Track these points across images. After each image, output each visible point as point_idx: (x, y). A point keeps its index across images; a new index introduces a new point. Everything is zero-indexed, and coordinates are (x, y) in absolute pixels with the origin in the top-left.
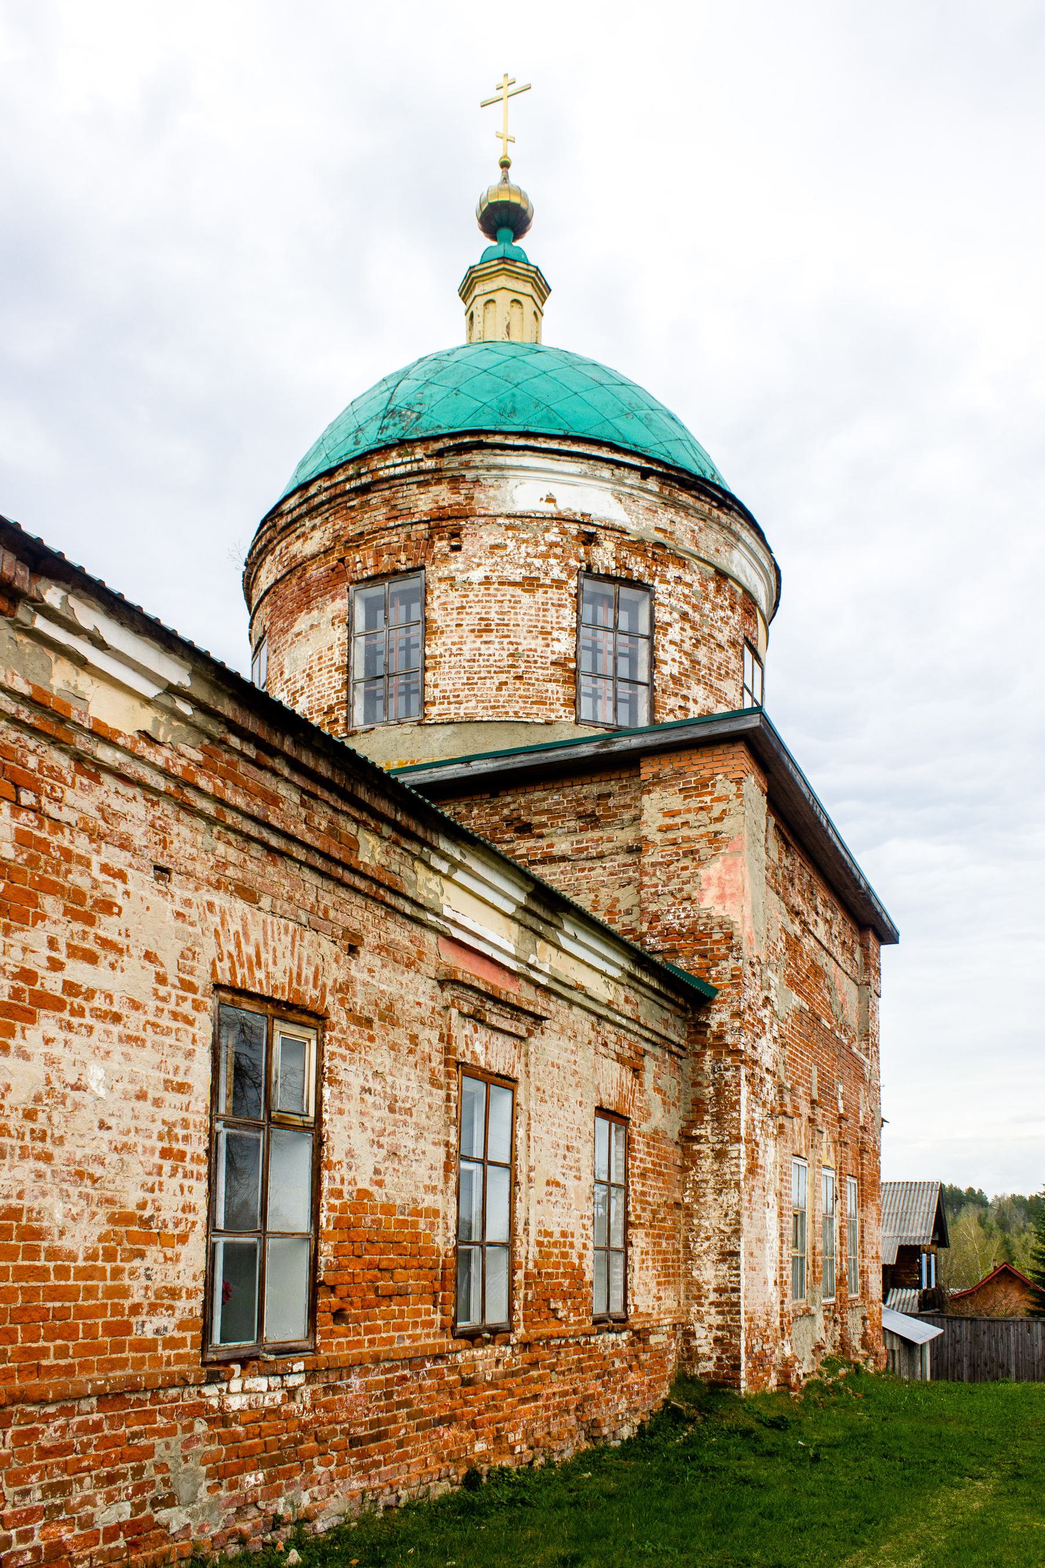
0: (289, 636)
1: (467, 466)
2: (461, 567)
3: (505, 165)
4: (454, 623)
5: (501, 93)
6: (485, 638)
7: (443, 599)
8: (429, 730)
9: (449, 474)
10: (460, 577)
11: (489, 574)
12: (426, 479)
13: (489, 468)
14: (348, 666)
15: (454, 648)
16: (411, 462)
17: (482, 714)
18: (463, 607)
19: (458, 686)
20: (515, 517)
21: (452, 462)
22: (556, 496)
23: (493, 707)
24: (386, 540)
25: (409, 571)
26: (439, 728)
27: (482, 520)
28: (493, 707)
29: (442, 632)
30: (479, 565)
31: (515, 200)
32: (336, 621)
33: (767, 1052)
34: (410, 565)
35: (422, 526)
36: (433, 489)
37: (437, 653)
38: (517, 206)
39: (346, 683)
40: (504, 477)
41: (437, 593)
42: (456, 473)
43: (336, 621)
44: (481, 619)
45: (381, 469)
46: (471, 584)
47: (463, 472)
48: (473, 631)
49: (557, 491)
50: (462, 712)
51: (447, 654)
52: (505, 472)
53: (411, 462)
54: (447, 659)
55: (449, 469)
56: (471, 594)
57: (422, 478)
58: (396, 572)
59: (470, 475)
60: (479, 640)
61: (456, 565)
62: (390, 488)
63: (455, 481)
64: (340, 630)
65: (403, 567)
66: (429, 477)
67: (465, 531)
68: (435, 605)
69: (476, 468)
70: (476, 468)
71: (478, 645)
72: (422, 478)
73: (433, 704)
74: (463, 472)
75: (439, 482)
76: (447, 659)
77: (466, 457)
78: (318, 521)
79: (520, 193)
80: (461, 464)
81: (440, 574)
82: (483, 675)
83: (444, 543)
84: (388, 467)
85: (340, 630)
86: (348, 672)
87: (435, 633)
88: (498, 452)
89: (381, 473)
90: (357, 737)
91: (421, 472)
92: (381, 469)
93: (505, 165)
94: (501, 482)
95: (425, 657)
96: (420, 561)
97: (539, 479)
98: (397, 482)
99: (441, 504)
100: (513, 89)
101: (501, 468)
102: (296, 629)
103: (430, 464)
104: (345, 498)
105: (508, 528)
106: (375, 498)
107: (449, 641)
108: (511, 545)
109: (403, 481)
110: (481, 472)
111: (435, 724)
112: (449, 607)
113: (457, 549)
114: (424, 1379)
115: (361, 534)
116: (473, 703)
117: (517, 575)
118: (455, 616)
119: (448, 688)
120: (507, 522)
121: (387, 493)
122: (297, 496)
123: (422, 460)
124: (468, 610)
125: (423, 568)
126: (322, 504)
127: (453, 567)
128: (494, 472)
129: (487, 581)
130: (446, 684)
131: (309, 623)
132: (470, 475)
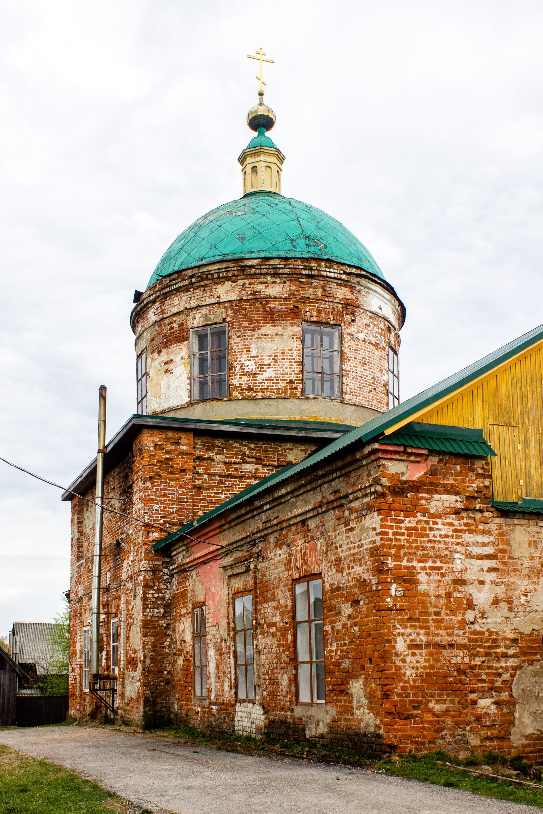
0: (256, 333)
1: (359, 283)
2: (356, 331)
3: (261, 94)
4: (353, 357)
5: (257, 56)
6: (364, 367)
7: (349, 344)
8: (345, 406)
9: (351, 284)
10: (355, 335)
11: (365, 337)
12: (343, 283)
13: (365, 287)
14: (302, 362)
15: (354, 369)
16: (337, 273)
17: (365, 404)
18: (357, 350)
19: (356, 388)
20: (373, 313)
21: (354, 280)
22: (382, 308)
23: (368, 401)
24: (323, 306)
25: (333, 325)
26: (349, 406)
27: (362, 311)
28: (368, 401)
29: (349, 360)
30: (362, 332)
31: (271, 116)
32: (295, 337)
33: (138, 496)
34: (335, 322)
35: (340, 305)
36: (343, 288)
37: (347, 369)
38: (272, 119)
39: (302, 371)
40: (369, 293)
41: (347, 340)
42: (353, 285)
43: (295, 337)
44: (363, 358)
45: (323, 271)
46: (359, 340)
47: (356, 286)
48: (360, 362)
49: (383, 306)
50: (357, 401)
51: (352, 371)
52: (369, 291)
53: (337, 273)
54: (351, 373)
55: (352, 282)
56: (359, 344)
57: (339, 282)
58: (327, 323)
59: (358, 287)
60: (363, 368)
61: (353, 329)
62: (324, 281)
63: (352, 288)
64: (297, 342)
65: (332, 322)
66: (342, 282)
67: (356, 314)
68: (346, 345)
69: (362, 286)
70: (362, 286)
71: (362, 370)
72: (339, 282)
73: (346, 394)
74: (356, 286)
75: (345, 286)
76: (351, 373)
77: (359, 280)
78: (278, 280)
79: (269, 110)
80: (357, 282)
81: (348, 331)
82: (364, 385)
83: (348, 317)
84: (326, 271)
85: (297, 342)
86: (303, 366)
87: (346, 359)
88: (370, 282)
89: (322, 272)
90: (310, 401)
91: (341, 279)
92: (323, 271)
93: (261, 94)
94: (367, 295)
95: (342, 370)
96: (339, 322)
97: (378, 298)
98: (328, 279)
99: (346, 297)
100: (264, 57)
101: (369, 288)
102: (263, 331)
103: (344, 277)
104: (299, 276)
105: (371, 317)
106: (316, 283)
107: (352, 365)
108: (372, 325)
109: (331, 280)
110: (362, 288)
111: (349, 404)
112: (352, 348)
113: (353, 321)
114: (178, 704)
115: (308, 298)
116: (361, 398)
117: (373, 341)
118: (354, 353)
119: (353, 387)
120: (371, 314)
121: (322, 283)
122: (259, 260)
123: (342, 274)
124: (359, 352)
125: (340, 325)
126: (285, 274)
127: (353, 329)
128: (366, 290)
129: (364, 340)
130: (351, 385)
131: (275, 332)
132: (358, 287)
